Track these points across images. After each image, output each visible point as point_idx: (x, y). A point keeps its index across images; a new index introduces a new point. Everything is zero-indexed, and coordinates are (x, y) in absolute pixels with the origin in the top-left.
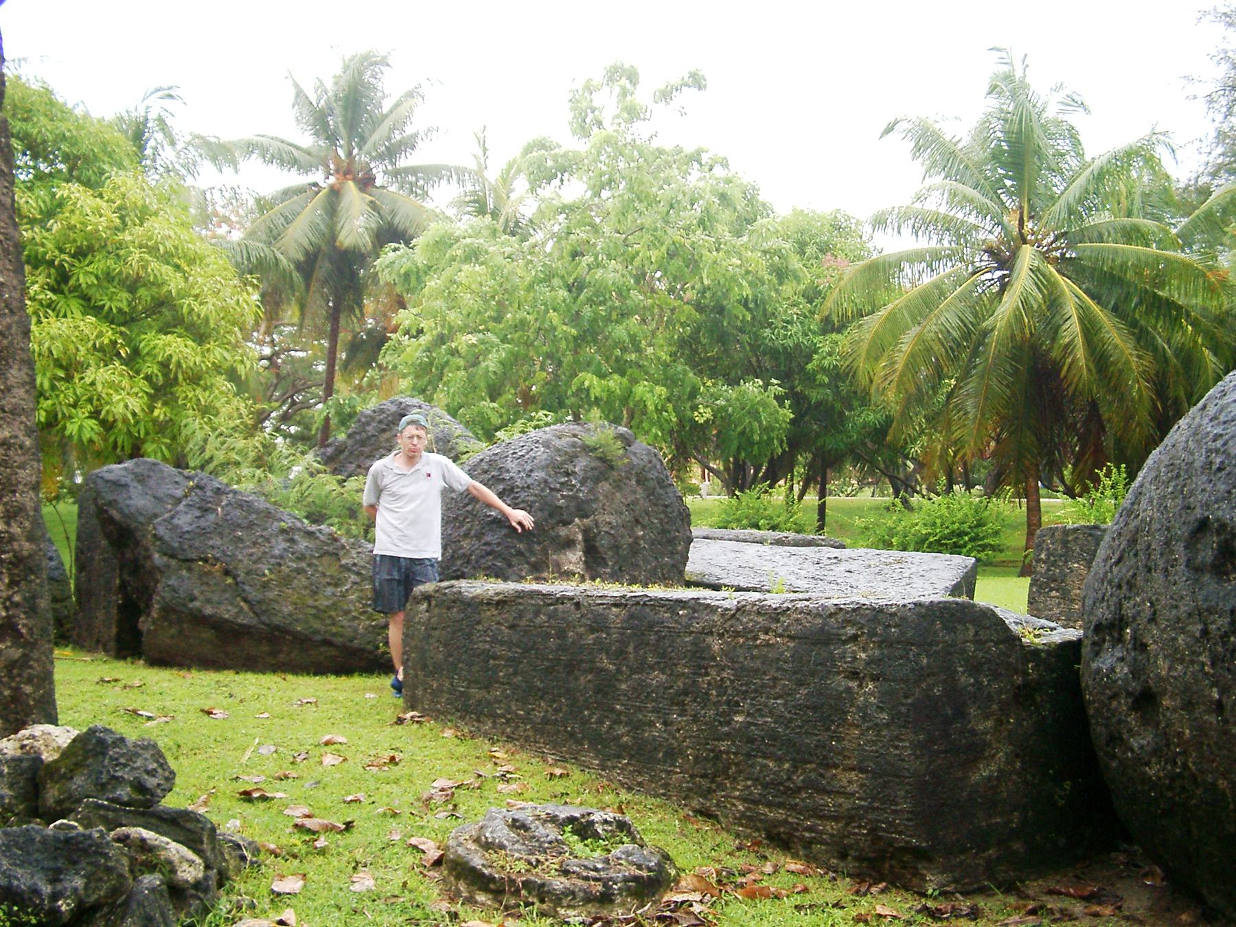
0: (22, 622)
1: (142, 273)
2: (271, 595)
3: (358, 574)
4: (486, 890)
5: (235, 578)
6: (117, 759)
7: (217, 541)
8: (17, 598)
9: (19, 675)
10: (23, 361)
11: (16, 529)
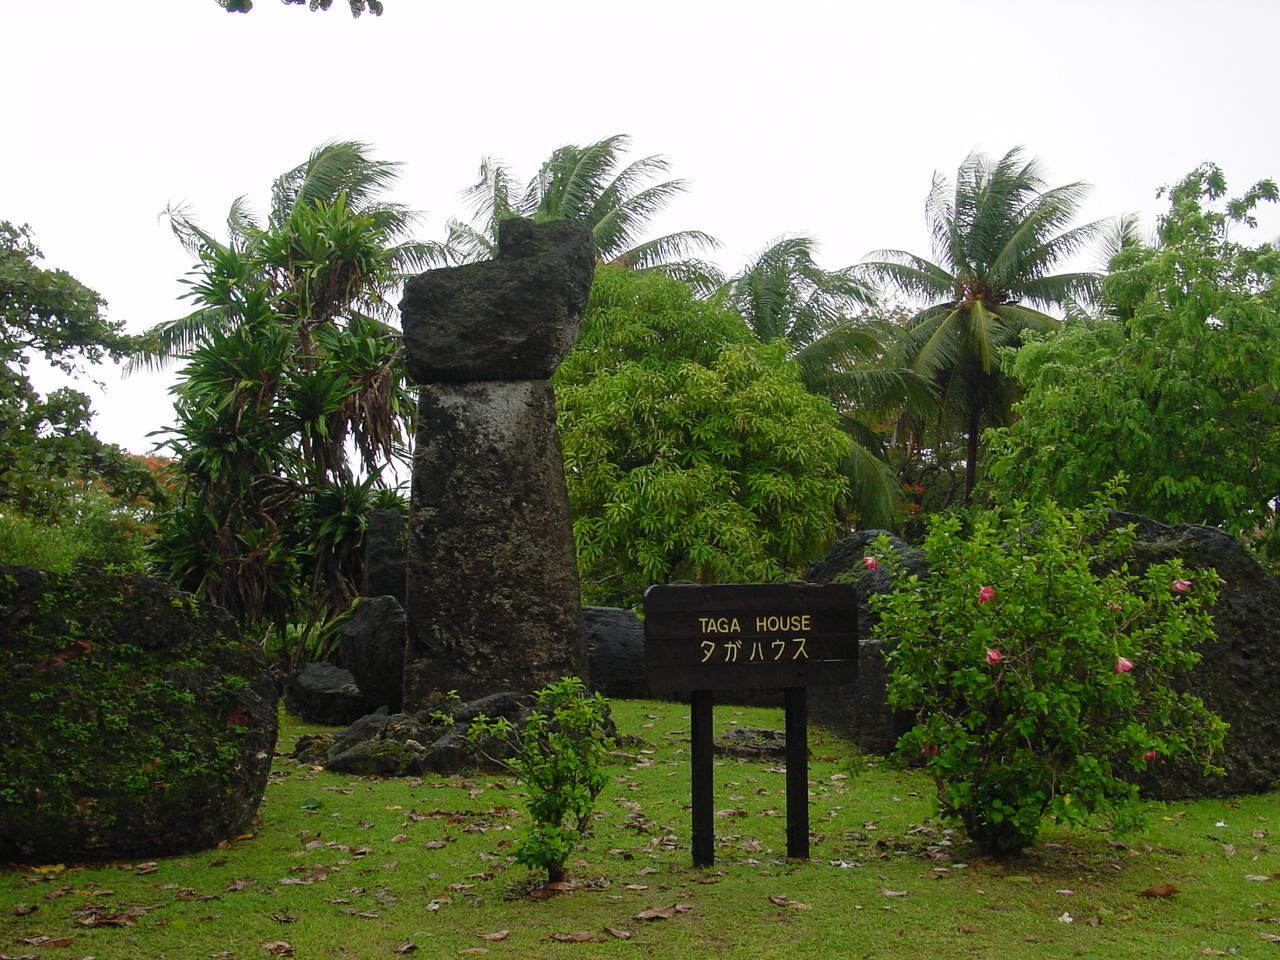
0: (573, 659)
11: (569, 618)
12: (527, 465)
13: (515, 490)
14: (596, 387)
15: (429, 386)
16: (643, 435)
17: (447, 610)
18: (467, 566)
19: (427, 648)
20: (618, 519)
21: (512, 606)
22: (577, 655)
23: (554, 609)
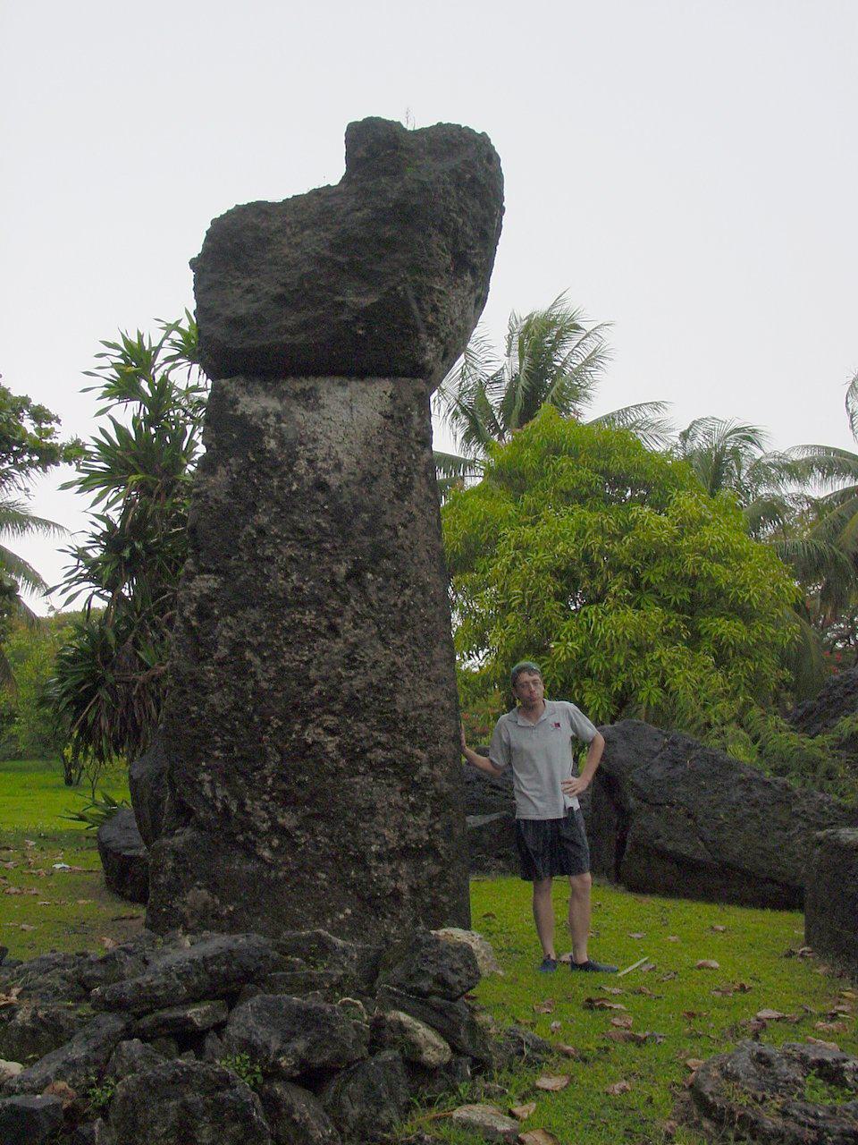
0: (441, 844)
1: (697, 572)
2: (724, 836)
3: (806, 820)
4: (709, 1116)
5: (695, 820)
6: (427, 956)
7: (682, 789)
8: (438, 826)
9: (438, 887)
10: (445, 642)
11: (438, 772)
12: (377, 514)
13: (354, 552)
14: (544, 530)
15: (223, 382)
16: (592, 576)
17: (228, 749)
18: (264, 675)
19: (190, 813)
20: (565, 658)
21: (339, 747)
22: (449, 836)
23: (411, 755)
